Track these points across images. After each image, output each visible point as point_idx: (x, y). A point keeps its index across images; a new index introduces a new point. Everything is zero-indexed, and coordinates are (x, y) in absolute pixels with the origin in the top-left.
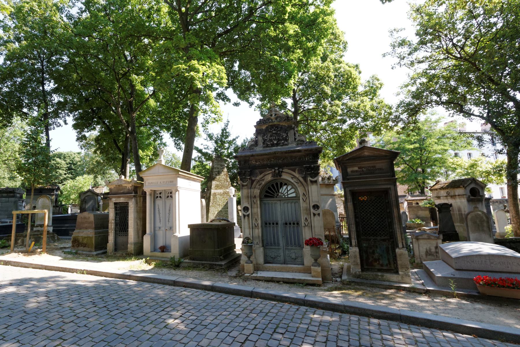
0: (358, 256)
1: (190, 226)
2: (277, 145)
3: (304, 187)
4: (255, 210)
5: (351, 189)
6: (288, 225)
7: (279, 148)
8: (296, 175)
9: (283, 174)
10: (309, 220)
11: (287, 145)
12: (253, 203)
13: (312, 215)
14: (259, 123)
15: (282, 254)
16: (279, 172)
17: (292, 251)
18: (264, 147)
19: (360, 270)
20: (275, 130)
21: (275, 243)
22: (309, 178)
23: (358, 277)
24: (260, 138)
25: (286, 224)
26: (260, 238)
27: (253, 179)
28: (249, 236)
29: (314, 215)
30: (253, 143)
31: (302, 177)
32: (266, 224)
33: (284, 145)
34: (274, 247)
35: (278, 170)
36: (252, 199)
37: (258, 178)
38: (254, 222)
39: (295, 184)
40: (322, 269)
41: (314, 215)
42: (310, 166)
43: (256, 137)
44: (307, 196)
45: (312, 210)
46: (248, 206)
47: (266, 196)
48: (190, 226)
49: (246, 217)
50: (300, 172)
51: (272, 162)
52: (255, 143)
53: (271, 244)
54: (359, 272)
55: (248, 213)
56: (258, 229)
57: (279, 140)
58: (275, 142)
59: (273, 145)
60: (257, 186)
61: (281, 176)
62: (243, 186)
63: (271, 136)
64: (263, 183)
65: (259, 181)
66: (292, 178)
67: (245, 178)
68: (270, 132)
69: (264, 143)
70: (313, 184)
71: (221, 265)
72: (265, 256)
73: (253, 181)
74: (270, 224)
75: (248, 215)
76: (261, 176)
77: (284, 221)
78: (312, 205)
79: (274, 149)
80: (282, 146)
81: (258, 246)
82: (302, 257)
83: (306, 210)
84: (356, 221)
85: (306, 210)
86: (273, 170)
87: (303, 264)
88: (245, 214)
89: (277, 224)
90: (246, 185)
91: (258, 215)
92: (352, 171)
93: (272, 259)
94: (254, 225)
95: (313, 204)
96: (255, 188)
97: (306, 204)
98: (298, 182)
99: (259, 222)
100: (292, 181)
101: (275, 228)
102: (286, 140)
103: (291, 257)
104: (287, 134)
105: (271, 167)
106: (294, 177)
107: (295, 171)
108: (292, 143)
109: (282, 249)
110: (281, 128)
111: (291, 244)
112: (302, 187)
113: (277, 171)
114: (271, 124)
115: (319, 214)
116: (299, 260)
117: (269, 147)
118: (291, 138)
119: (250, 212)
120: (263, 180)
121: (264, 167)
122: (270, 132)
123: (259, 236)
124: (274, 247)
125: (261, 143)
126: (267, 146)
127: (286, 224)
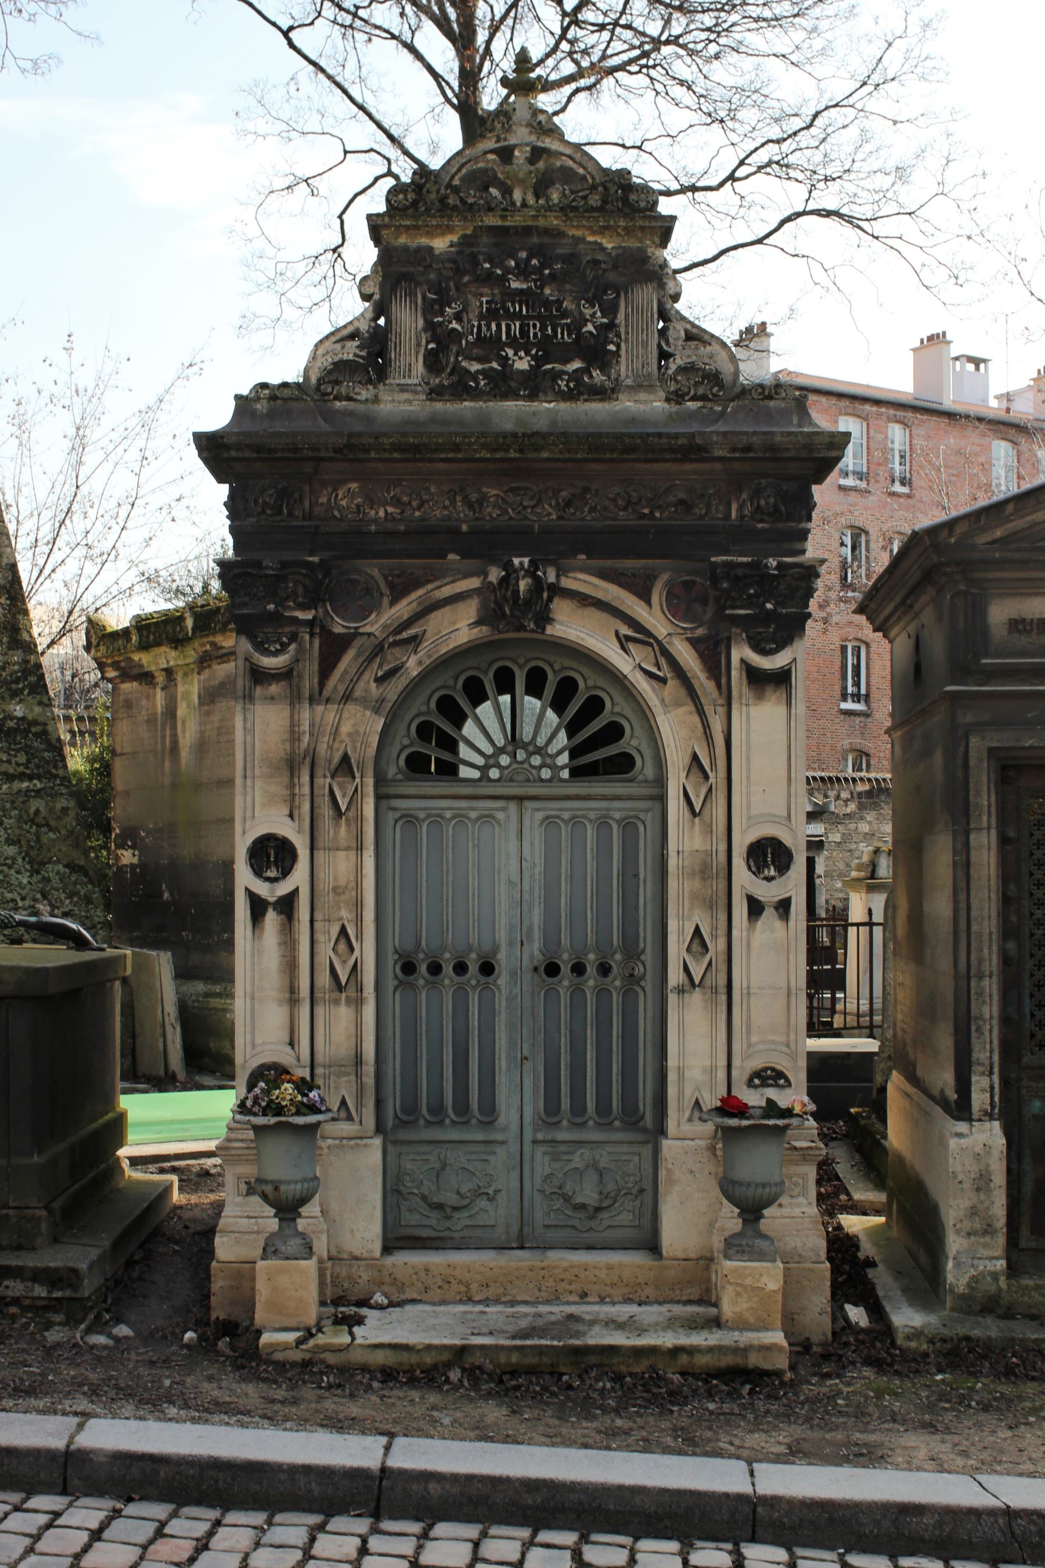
0: (999, 1178)
1: (673, 219)
2: (534, 385)
3: (701, 713)
4: (338, 866)
5: (997, 739)
6: (566, 979)
7: (546, 411)
8: (655, 619)
9: (561, 608)
10: (717, 947)
11: (600, 393)
12: (326, 811)
13: (740, 909)
14: (415, 200)
15: (507, 1182)
16: (538, 584)
17: (578, 1159)
18: (435, 393)
19: (1001, 1264)
20: (523, 271)
21: (462, 1106)
22: (741, 653)
23: (990, 1306)
24: (408, 320)
25: (552, 970)
26: (369, 1069)
27: (339, 626)
28: (284, 1057)
29: (755, 908)
30: (351, 351)
31: (694, 642)
32: (409, 968)
33: (580, 390)
34: (453, 1135)
35: (531, 573)
36: (323, 782)
37: (375, 625)
38: (326, 951)
39: (643, 685)
40: (787, 1273)
41: (755, 908)
42: (756, 566)
43: (381, 309)
44: (717, 778)
45: (743, 877)
46: (286, 829)
47: (417, 765)
48: (673, 219)
49: (271, 918)
50: (680, 604)
51: (491, 511)
52: (361, 357)
53: (437, 1110)
54: (995, 1276)
55: (284, 888)
56: (358, 1003)
57: (547, 350)
58: (522, 364)
59: (503, 384)
60: (368, 686)
61: (544, 618)
62: (258, 676)
63: (492, 314)
64: (413, 665)
65: (379, 650)
66: (623, 642)
67: (276, 618)
68: (488, 278)
69: (433, 362)
70: (760, 696)
71: (68, 1278)
72: (394, 1192)
73: (333, 648)
74: (435, 969)
75: (287, 905)
76: (403, 609)
77: (535, 950)
78: (742, 841)
79: (510, 412)
80: (570, 396)
81: (345, 1128)
82: (648, 1196)
83: (704, 871)
84: (1006, 960)
85: (704, 871)
86: (495, 574)
87: (652, 1246)
88: (262, 889)
89: (487, 968)
90: (286, 675)
91: (358, 905)
92: (1016, 625)
93: (433, 1218)
94: (324, 979)
95: (752, 836)
96: (347, 698)
97: (708, 830)
98: (666, 671)
99: (367, 951)
100: (622, 663)
101: (474, 1000)
102: (597, 353)
103: (567, 1198)
104: (610, 310)
105: (483, 545)
106: (638, 635)
107: (645, 597)
108: (641, 386)
109: (514, 1147)
110: (571, 259)
111: (578, 1108)
112: (686, 713)
113: (523, 585)
114: (492, 220)
115: (784, 907)
116: (624, 1217)
117: (475, 394)
118: (633, 358)
119: (299, 877)
120: (415, 641)
121: (420, 551)
122: (488, 278)
123: (358, 1060)
124: (453, 1135)
125: (410, 363)
126: (461, 387)
127: (552, 970)
